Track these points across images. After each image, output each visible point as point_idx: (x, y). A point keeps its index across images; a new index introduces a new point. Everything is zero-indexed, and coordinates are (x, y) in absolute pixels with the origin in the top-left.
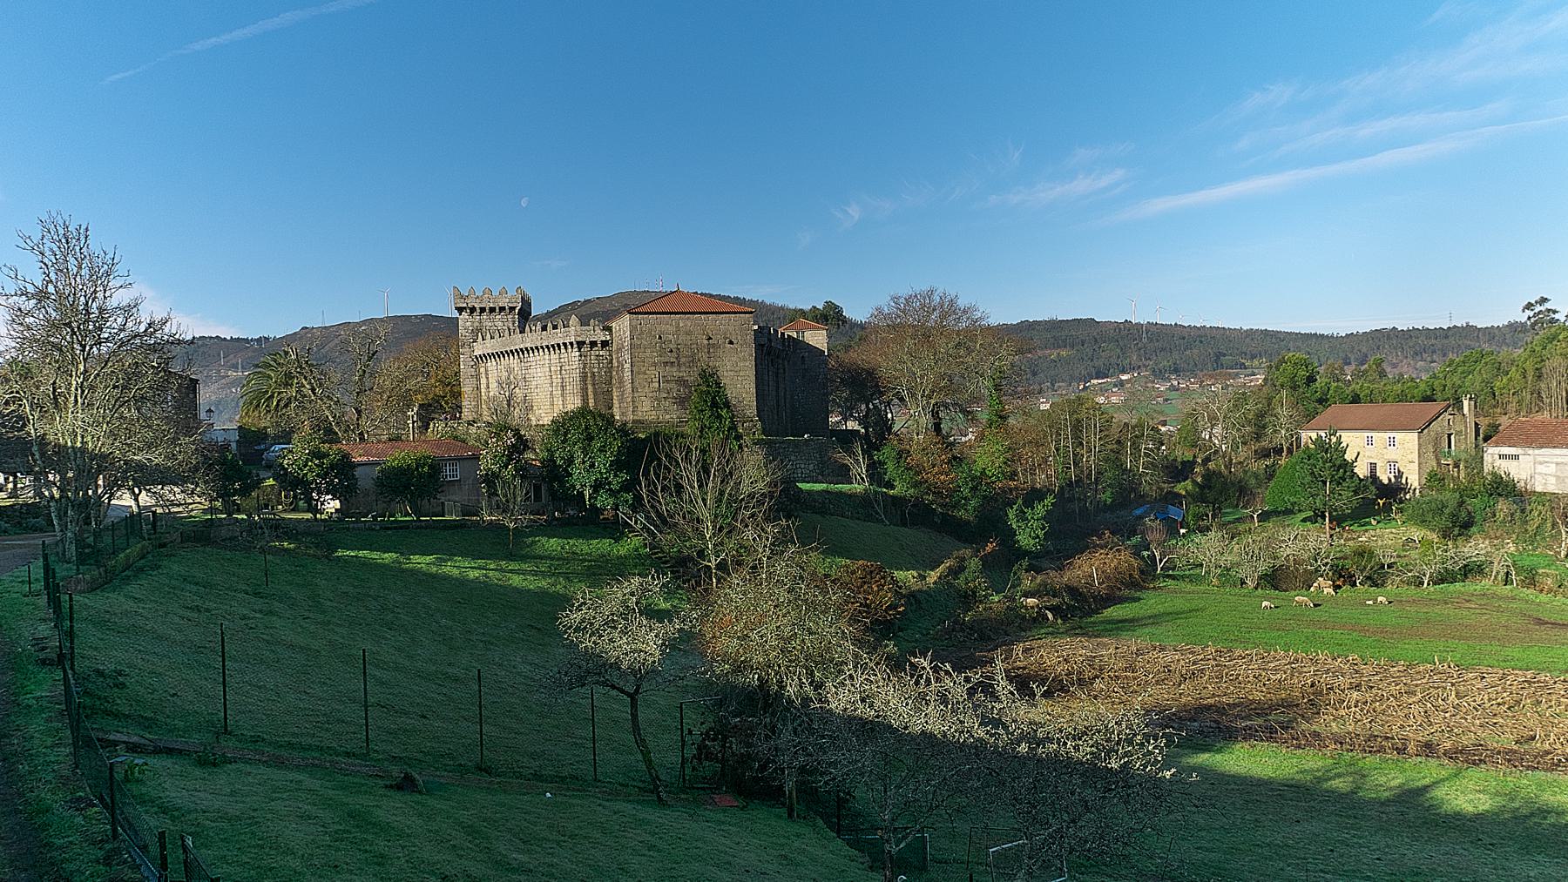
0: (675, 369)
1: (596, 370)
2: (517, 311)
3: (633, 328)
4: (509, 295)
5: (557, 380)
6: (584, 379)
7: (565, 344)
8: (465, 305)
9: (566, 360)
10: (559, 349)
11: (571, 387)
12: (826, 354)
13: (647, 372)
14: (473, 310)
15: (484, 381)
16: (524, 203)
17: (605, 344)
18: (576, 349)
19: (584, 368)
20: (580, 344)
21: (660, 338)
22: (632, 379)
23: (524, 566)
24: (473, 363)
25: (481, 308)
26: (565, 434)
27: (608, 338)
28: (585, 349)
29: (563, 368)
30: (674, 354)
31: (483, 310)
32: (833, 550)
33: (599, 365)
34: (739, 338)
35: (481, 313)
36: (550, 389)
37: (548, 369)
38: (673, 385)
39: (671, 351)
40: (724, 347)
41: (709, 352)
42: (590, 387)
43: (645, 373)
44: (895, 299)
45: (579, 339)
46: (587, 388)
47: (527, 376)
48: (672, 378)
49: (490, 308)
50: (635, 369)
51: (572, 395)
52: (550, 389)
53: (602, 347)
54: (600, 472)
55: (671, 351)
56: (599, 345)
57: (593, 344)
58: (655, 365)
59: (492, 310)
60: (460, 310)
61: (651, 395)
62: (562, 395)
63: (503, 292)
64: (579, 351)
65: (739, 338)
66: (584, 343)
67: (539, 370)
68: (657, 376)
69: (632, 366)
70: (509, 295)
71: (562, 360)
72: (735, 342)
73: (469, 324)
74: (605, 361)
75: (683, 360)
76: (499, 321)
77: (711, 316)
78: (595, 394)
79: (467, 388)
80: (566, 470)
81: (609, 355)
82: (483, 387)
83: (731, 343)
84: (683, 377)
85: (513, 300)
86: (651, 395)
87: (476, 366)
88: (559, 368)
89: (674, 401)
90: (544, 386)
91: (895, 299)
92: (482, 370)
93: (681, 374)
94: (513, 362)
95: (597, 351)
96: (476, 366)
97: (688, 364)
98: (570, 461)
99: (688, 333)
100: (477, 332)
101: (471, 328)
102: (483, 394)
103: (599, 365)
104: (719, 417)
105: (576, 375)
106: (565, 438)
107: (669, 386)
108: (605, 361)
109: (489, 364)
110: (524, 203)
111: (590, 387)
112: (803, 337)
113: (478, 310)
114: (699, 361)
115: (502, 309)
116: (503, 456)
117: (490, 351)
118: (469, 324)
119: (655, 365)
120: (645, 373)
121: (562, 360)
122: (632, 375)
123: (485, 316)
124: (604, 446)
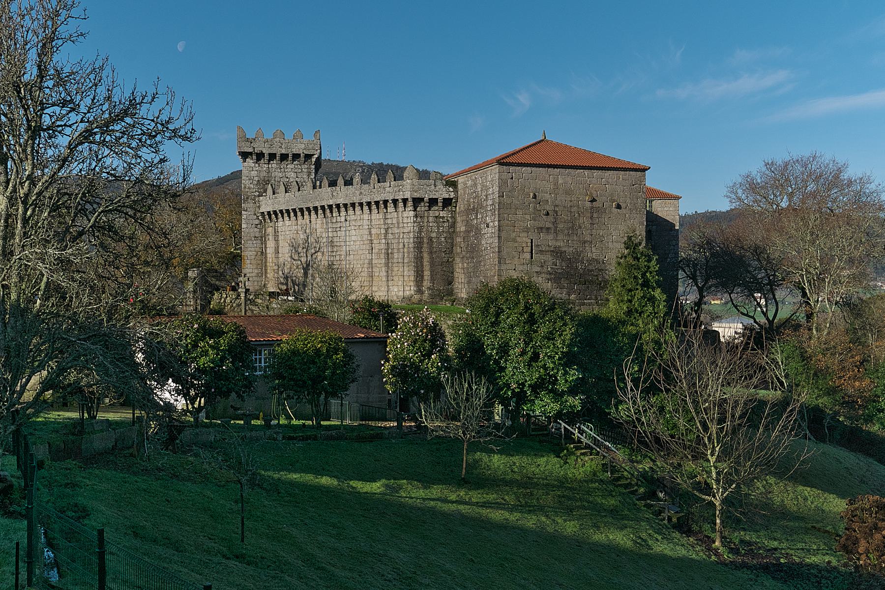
0: (551, 237)
1: (434, 235)
2: (314, 160)
3: (503, 184)
4: (305, 140)
5: (380, 245)
6: (419, 244)
7: (395, 201)
8: (250, 150)
9: (395, 221)
10: (296, 215)
11: (401, 255)
12: (677, 228)
13: (518, 239)
14: (260, 156)
15: (271, 244)
16: (180, 47)
17: (447, 202)
18: (411, 208)
19: (420, 232)
20: (417, 201)
21: (535, 197)
22: (499, 247)
23: (492, 497)
24: (257, 222)
25: (270, 154)
26: (497, 315)
27: (452, 195)
28: (422, 208)
29: (390, 231)
30: (551, 218)
31: (272, 156)
32: (353, 488)
33: (438, 229)
34: (628, 201)
35: (269, 161)
36: (369, 257)
37: (367, 232)
38: (549, 258)
39: (548, 214)
40: (611, 212)
41: (592, 218)
42: (426, 256)
43: (514, 240)
44: (769, 165)
45: (417, 195)
46: (422, 258)
47: (335, 240)
48: (547, 248)
49: (282, 155)
50: (503, 234)
51: (401, 265)
52: (369, 257)
53: (444, 207)
54: (544, 367)
55: (548, 214)
56: (440, 204)
57: (433, 202)
58: (527, 230)
59: (284, 157)
60: (245, 155)
61: (521, 268)
62: (387, 265)
63: (298, 136)
64: (415, 210)
65: (628, 201)
66: (422, 200)
67: (353, 232)
68: (529, 244)
69: (499, 230)
70: (305, 140)
71: (389, 221)
72: (623, 205)
73: (254, 173)
74: (446, 225)
75: (561, 226)
76: (291, 171)
77: (596, 173)
78: (432, 263)
79: (249, 253)
80: (497, 362)
81: (451, 217)
82: (270, 251)
83: (619, 207)
84: (560, 247)
85: (310, 147)
86: (521, 268)
87: (261, 225)
88: (383, 231)
89: (548, 276)
90: (360, 252)
91: (769, 165)
92: (270, 230)
93: (558, 244)
94: (318, 222)
95: (436, 211)
96: (261, 225)
97: (566, 231)
98: (504, 350)
99: (568, 192)
100: (264, 184)
101: (256, 179)
102: (269, 260)
103: (438, 229)
104: (652, 299)
105: (409, 240)
106: (496, 320)
107: (543, 258)
108: (446, 225)
109: (280, 223)
110: (180, 47)
111: (426, 256)
112: (651, 206)
113: (267, 157)
114: (580, 227)
115: (296, 156)
116: (425, 341)
117: (284, 208)
118: (254, 173)
119: (527, 230)
120: (514, 240)
121: (389, 221)
122: (499, 242)
123: (274, 164)
124: (551, 333)
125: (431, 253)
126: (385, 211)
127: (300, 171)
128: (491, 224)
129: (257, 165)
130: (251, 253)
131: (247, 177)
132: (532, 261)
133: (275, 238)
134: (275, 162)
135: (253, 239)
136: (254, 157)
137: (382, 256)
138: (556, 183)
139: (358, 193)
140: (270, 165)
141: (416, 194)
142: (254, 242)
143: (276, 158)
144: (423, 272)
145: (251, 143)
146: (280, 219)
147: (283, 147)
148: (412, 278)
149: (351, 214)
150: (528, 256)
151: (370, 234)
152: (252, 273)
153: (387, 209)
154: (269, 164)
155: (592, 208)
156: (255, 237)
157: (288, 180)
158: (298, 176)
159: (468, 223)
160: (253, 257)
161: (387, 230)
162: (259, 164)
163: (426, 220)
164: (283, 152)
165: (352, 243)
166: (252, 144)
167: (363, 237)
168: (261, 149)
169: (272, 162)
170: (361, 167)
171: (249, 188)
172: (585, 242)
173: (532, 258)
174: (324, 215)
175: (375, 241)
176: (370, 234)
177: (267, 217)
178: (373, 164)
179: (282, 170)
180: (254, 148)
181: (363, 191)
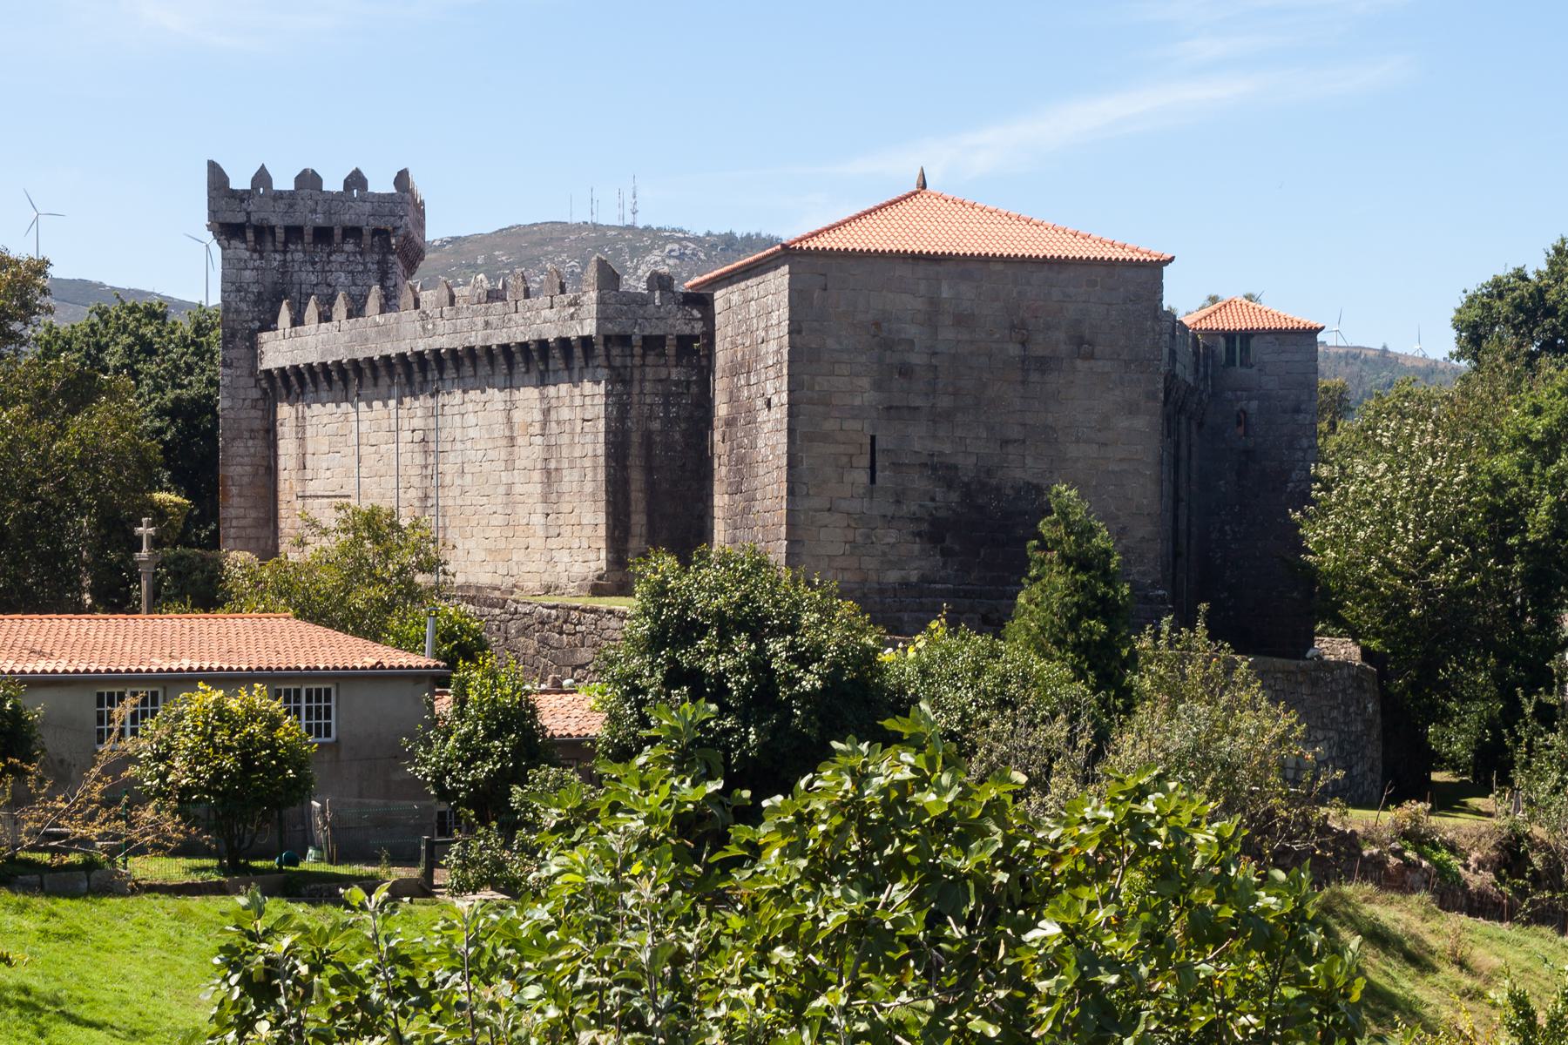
1: (656, 425)
8: (241, 218)
14: (263, 232)
27: (698, 328)
29: (553, 415)
31: (294, 233)
35: (285, 244)
37: (501, 417)
38: (919, 483)
57: (653, 343)
59: (323, 235)
78: (651, 490)
88: (538, 416)
93: (937, 447)
99: (962, 320)
101: (255, 289)
103: (667, 412)
111: (637, 478)
113: (280, 235)
115: (353, 232)
125: (649, 470)
126: (542, 367)
127: (361, 268)
128: (775, 400)
129: (256, 256)
130: (239, 469)
131: (233, 283)
132: (872, 492)
133: (297, 433)
134: (299, 247)
135: (246, 435)
136: (250, 235)
137: (537, 476)
138: (934, 303)
139: (480, 321)
140: (289, 257)
141: (610, 326)
142: (250, 443)
143: (302, 239)
144: (628, 515)
145: (242, 201)
146: (310, 387)
147: (319, 209)
148: (602, 531)
149: (468, 374)
150: (862, 477)
151: (509, 420)
152: (245, 517)
153: (547, 365)
154: (285, 252)
155: (1024, 360)
156: (252, 431)
157: (330, 291)
158: (358, 282)
159: (733, 399)
160: (246, 480)
161: (546, 412)
162: (261, 253)
163: (636, 390)
164: (320, 220)
165: (469, 444)
166: (244, 205)
167: (493, 430)
168: (262, 215)
169: (292, 247)
170: (678, 241)
171: (238, 311)
172: (1005, 442)
173: (873, 480)
174: (543, 429)
175: (520, 441)
176: (509, 420)
177: (279, 383)
178: (709, 234)
179: (318, 267)
180: (248, 214)
181: (491, 318)
